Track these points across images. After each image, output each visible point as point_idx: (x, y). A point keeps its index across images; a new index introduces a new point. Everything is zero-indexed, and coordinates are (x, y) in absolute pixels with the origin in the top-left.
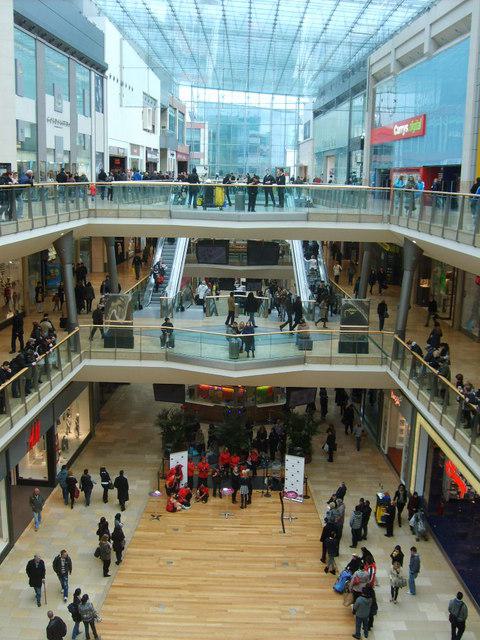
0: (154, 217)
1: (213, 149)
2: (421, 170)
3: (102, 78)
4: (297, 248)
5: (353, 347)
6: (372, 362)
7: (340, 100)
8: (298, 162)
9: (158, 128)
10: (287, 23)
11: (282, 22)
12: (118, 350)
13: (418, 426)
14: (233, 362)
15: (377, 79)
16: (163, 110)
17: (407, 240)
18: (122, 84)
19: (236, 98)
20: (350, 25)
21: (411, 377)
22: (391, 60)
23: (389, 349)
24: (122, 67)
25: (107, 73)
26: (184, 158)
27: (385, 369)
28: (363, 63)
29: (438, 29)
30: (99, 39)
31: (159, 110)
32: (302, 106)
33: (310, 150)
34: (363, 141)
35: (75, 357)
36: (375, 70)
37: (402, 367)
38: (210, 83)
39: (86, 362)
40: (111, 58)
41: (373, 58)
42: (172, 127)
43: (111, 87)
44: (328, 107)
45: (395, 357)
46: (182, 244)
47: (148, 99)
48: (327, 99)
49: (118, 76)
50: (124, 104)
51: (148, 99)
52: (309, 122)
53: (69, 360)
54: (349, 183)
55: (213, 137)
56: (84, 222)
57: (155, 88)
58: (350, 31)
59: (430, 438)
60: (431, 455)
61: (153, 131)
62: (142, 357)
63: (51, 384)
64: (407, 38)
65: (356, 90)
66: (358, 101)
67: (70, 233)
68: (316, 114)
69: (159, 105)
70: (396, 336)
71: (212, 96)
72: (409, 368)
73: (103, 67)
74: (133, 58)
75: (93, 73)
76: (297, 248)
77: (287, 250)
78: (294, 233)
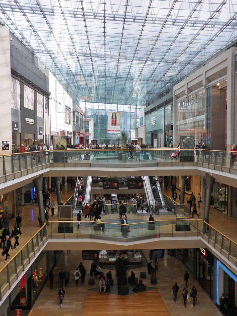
0: (82, 166)
1: (95, 131)
2: (150, 133)
3: (48, 98)
4: (146, 179)
5: (182, 228)
6: (193, 235)
7: (159, 107)
8: (138, 136)
9: (72, 123)
10: (123, 71)
11: (120, 71)
12: (66, 234)
13: (218, 267)
14: (124, 238)
15: (177, 97)
16: (74, 114)
17: (207, 174)
18: (56, 101)
19: (102, 106)
20: (152, 71)
21: (222, 247)
22: (185, 88)
23: (201, 228)
24: (56, 94)
25: (50, 97)
26: (83, 136)
27: (200, 238)
28: (168, 91)
29: (209, 74)
30: (45, 80)
31: (72, 113)
32: (138, 110)
33: (144, 130)
34: (172, 126)
35: (45, 238)
36: (177, 93)
37: (210, 237)
38: (93, 99)
39: (49, 241)
40: (51, 89)
41: (176, 87)
42: (78, 122)
43: (52, 103)
44: (153, 110)
45: (205, 232)
46: (90, 179)
47: (68, 108)
48: (150, 108)
49: (54, 98)
50: (57, 111)
51: (68, 108)
52: (142, 117)
53: (42, 240)
54: (165, 146)
55: (95, 125)
56: (48, 170)
57: (69, 102)
58: (164, 75)
59: (224, 272)
60: (227, 283)
61: (70, 123)
62: (78, 237)
63: (34, 253)
64: (196, 79)
65: (167, 103)
66: (169, 108)
67: (41, 175)
68: (146, 114)
69: (72, 111)
70: (204, 222)
71: (96, 106)
72: (213, 238)
73: (49, 94)
74: (61, 89)
75: (44, 97)
76: (146, 179)
77: (142, 181)
78: (145, 173)
